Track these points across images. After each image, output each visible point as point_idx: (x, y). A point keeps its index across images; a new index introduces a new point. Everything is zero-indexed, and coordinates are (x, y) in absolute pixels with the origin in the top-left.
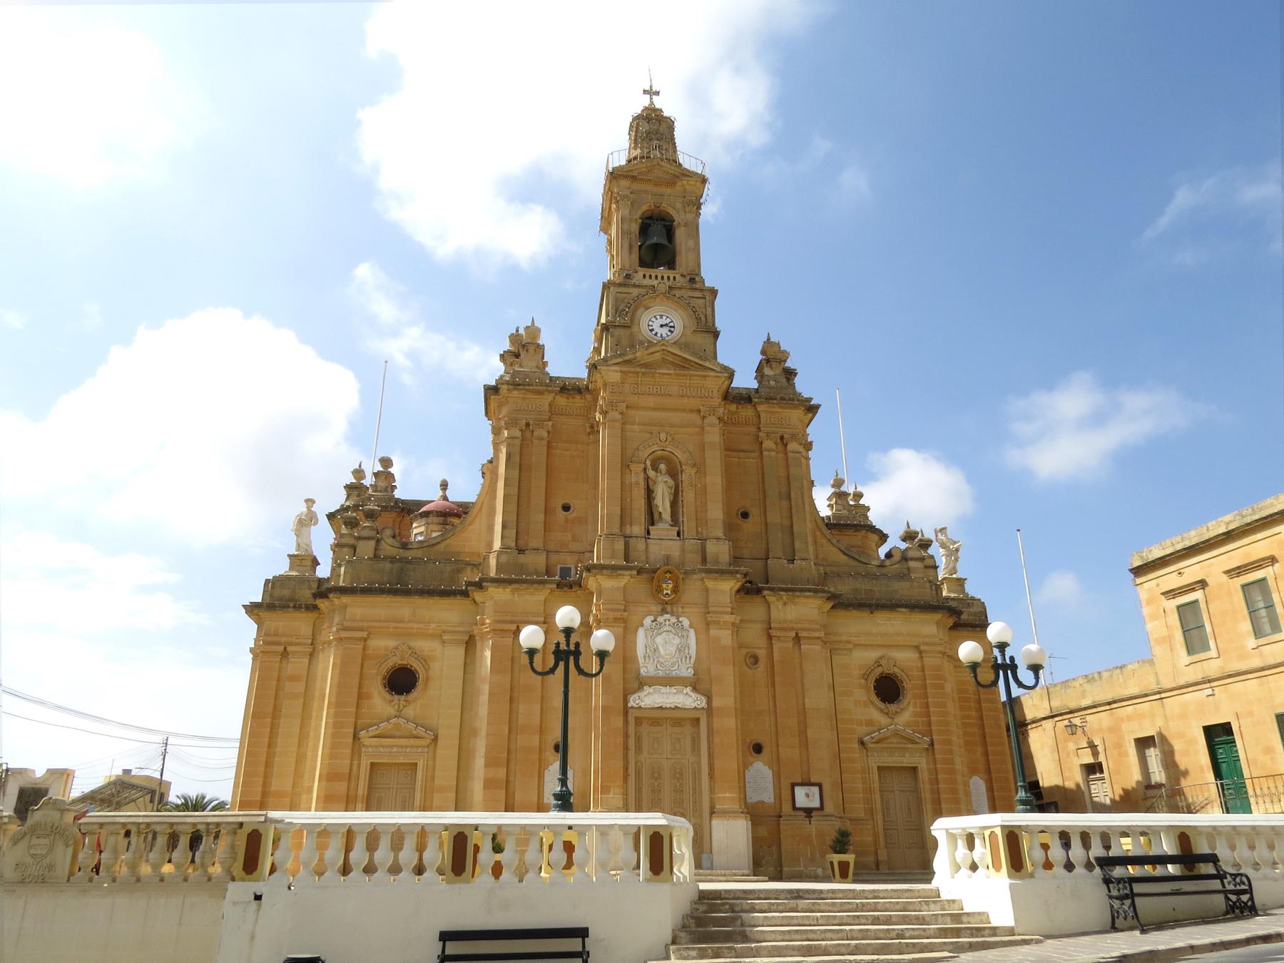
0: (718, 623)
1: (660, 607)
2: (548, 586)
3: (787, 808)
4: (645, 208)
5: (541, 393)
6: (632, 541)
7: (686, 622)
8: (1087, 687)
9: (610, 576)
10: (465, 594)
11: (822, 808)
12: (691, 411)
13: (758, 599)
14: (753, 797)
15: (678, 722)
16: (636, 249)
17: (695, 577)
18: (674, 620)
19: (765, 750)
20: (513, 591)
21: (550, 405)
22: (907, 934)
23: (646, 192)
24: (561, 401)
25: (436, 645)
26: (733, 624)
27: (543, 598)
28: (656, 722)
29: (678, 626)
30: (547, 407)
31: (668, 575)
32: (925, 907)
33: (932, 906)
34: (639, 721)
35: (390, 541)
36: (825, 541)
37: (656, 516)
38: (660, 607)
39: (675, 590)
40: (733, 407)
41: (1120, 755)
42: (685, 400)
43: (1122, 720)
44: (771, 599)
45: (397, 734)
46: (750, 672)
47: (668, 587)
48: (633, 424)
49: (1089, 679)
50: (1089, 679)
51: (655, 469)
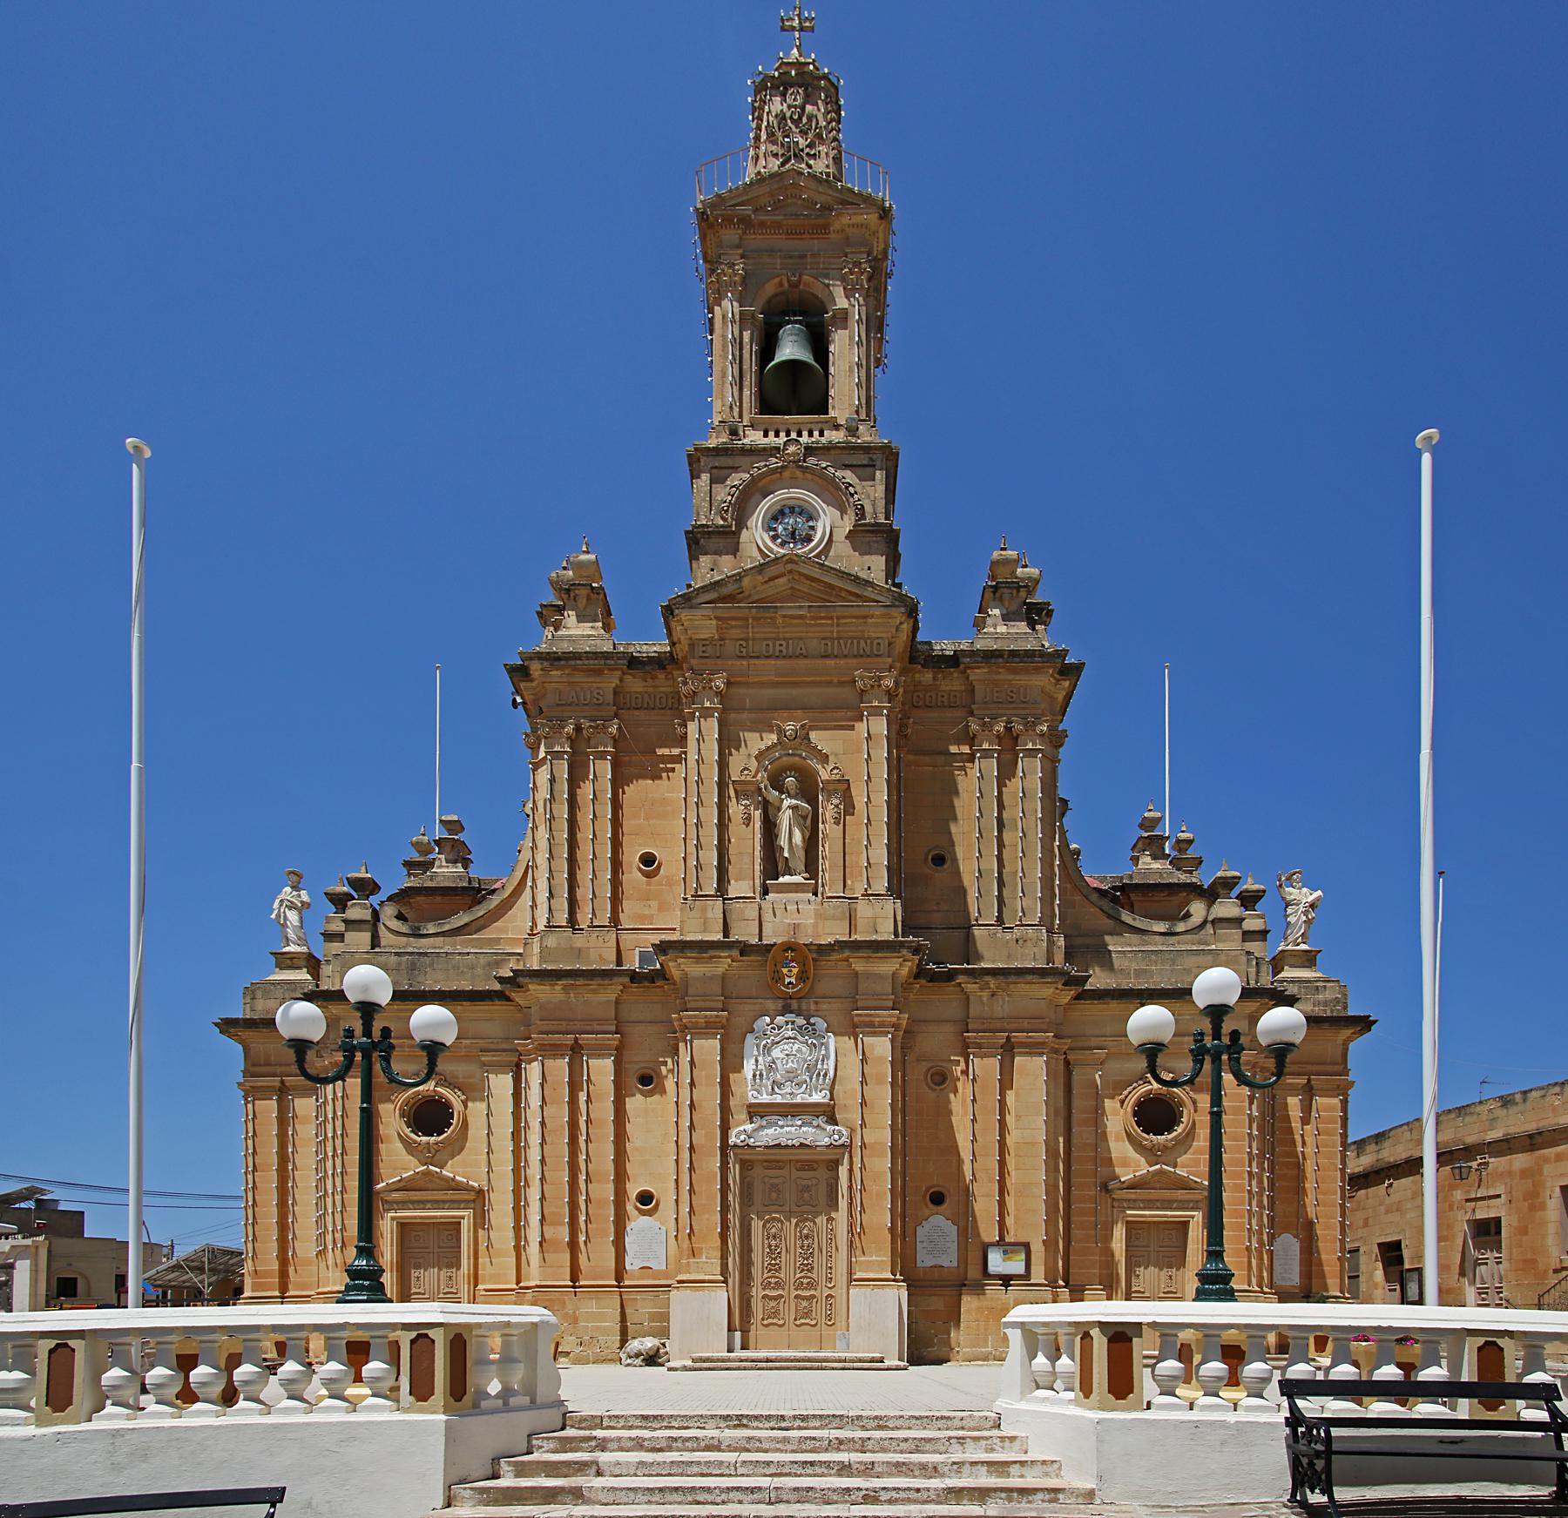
0: (871, 1025)
1: (780, 1004)
2: (616, 980)
3: (974, 1273)
4: (770, 289)
5: (598, 672)
6: (736, 906)
7: (821, 1024)
8: (1501, 1113)
9: (698, 960)
10: (501, 996)
11: (1027, 1275)
12: (841, 684)
13: (950, 988)
14: (924, 1260)
15: (808, 1165)
16: (750, 380)
17: (835, 956)
18: (801, 1021)
19: (947, 1201)
20: (565, 988)
21: (615, 692)
22: (884, 1496)
23: (771, 252)
24: (635, 684)
25: (472, 1068)
26: (896, 1026)
27: (613, 997)
28: (771, 1164)
29: (808, 1030)
30: (610, 697)
31: (790, 954)
32: (955, 1446)
33: (970, 1444)
34: (746, 1165)
35: (395, 924)
36: (1078, 898)
37: (781, 866)
38: (780, 1004)
39: (802, 977)
40: (927, 677)
41: (1532, 1208)
42: (831, 662)
43: (1546, 1160)
44: (970, 987)
45: (430, 1186)
46: (932, 1095)
47: (791, 974)
48: (742, 709)
49: (1506, 1101)
50: (1506, 1101)
51: (781, 789)
